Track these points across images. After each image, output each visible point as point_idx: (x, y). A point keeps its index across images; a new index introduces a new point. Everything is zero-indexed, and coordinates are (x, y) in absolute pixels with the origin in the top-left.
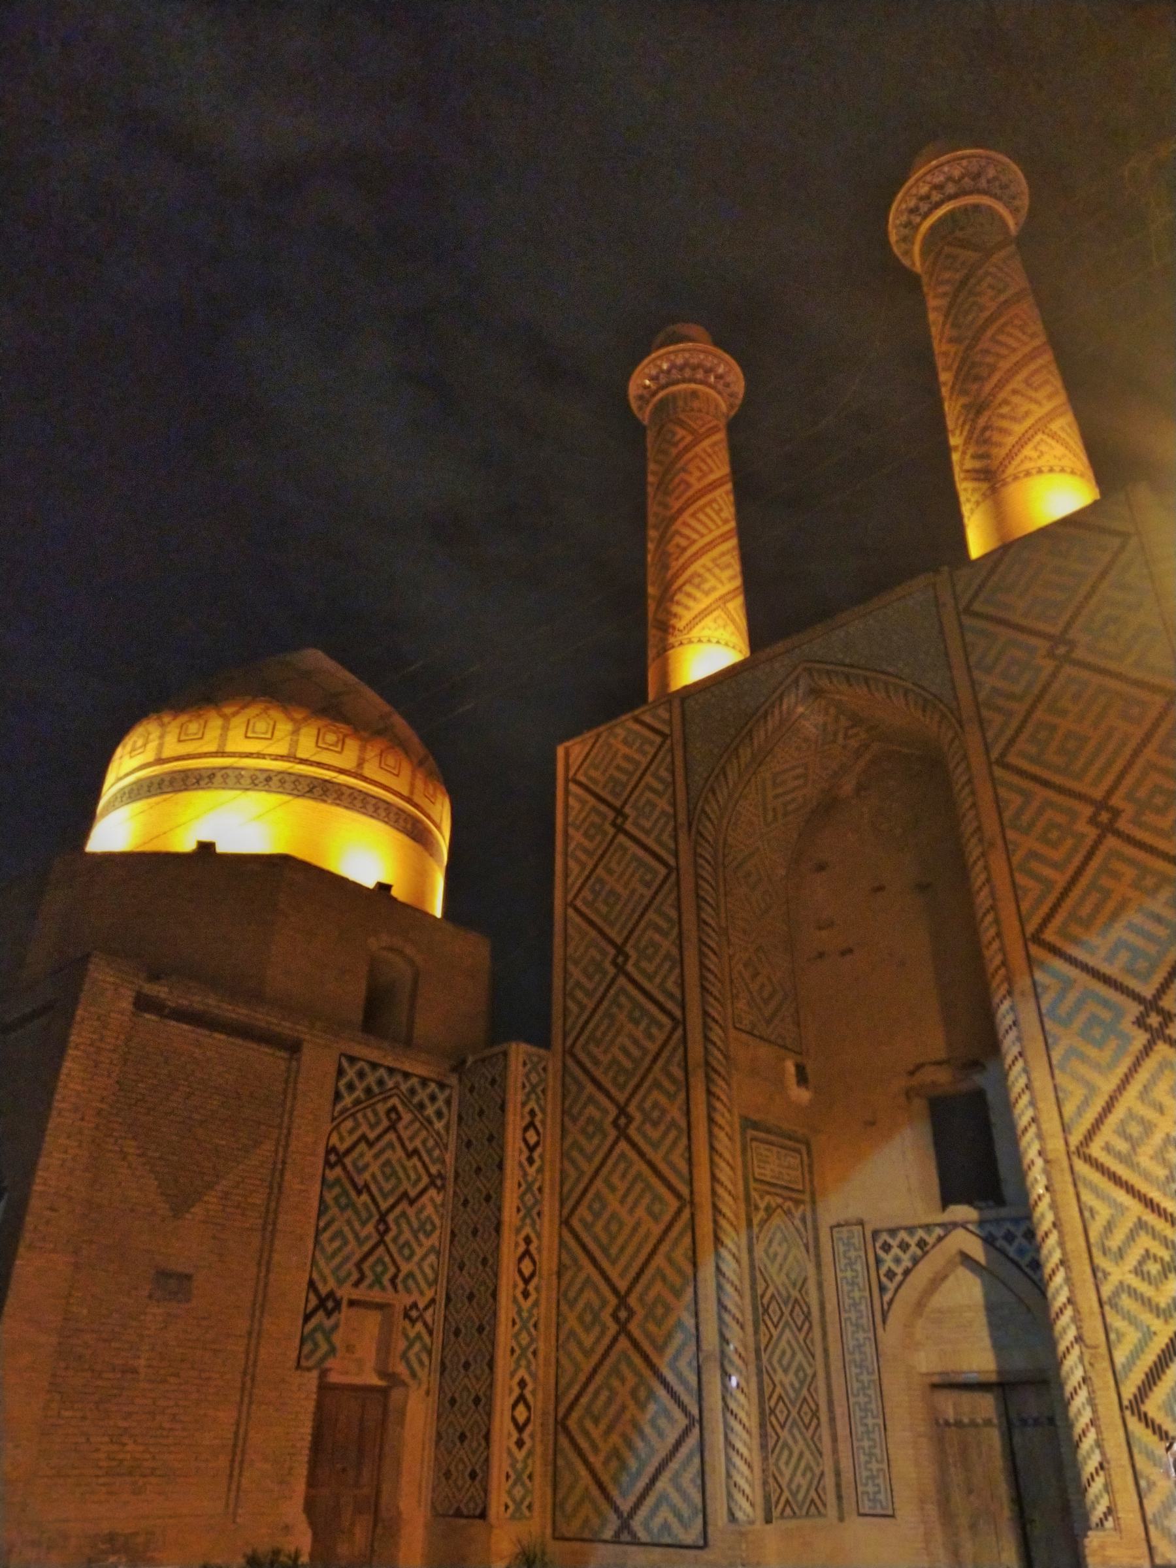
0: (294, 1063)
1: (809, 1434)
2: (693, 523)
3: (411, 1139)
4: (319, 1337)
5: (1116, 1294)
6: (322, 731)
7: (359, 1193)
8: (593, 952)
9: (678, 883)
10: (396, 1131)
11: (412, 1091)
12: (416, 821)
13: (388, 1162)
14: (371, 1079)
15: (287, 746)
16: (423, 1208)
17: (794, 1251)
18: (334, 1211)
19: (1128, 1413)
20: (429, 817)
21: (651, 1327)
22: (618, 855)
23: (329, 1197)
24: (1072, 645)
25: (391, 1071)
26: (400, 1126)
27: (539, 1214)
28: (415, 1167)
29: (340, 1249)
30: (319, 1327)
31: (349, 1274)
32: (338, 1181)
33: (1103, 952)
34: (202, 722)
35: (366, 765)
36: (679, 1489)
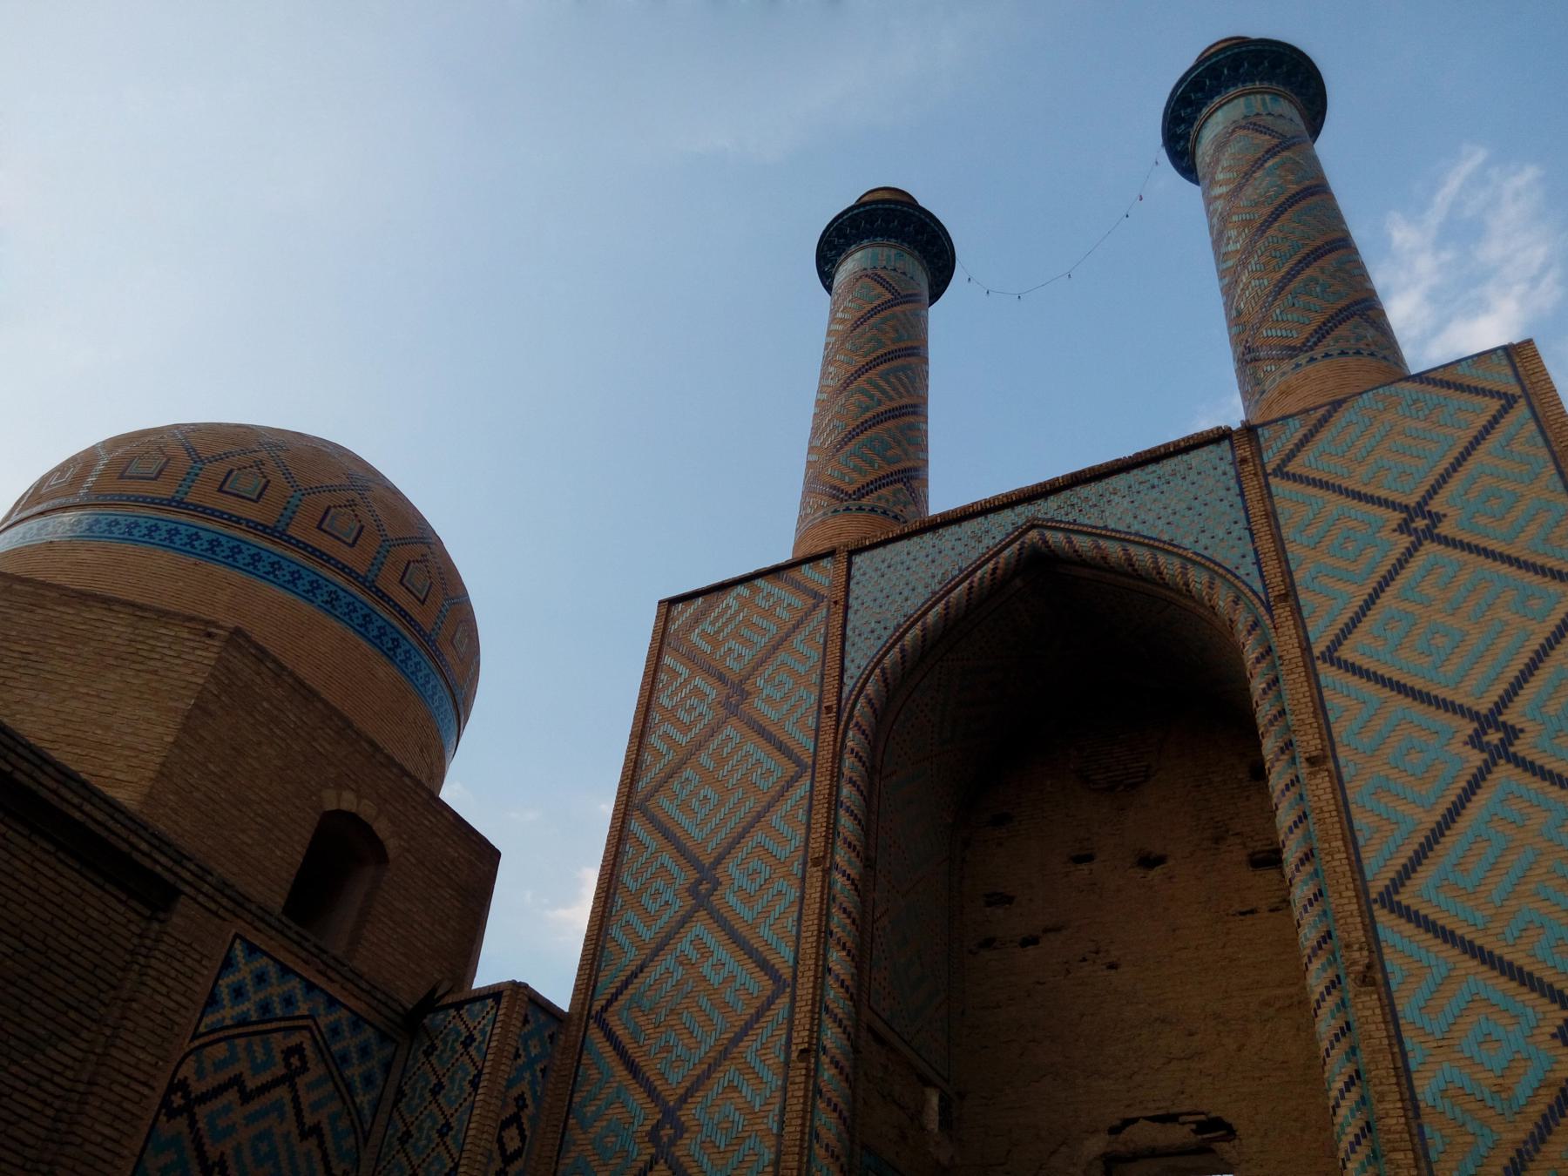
10: (293, 1088)
14: (276, 990)
25: (310, 987)
26: (301, 1081)
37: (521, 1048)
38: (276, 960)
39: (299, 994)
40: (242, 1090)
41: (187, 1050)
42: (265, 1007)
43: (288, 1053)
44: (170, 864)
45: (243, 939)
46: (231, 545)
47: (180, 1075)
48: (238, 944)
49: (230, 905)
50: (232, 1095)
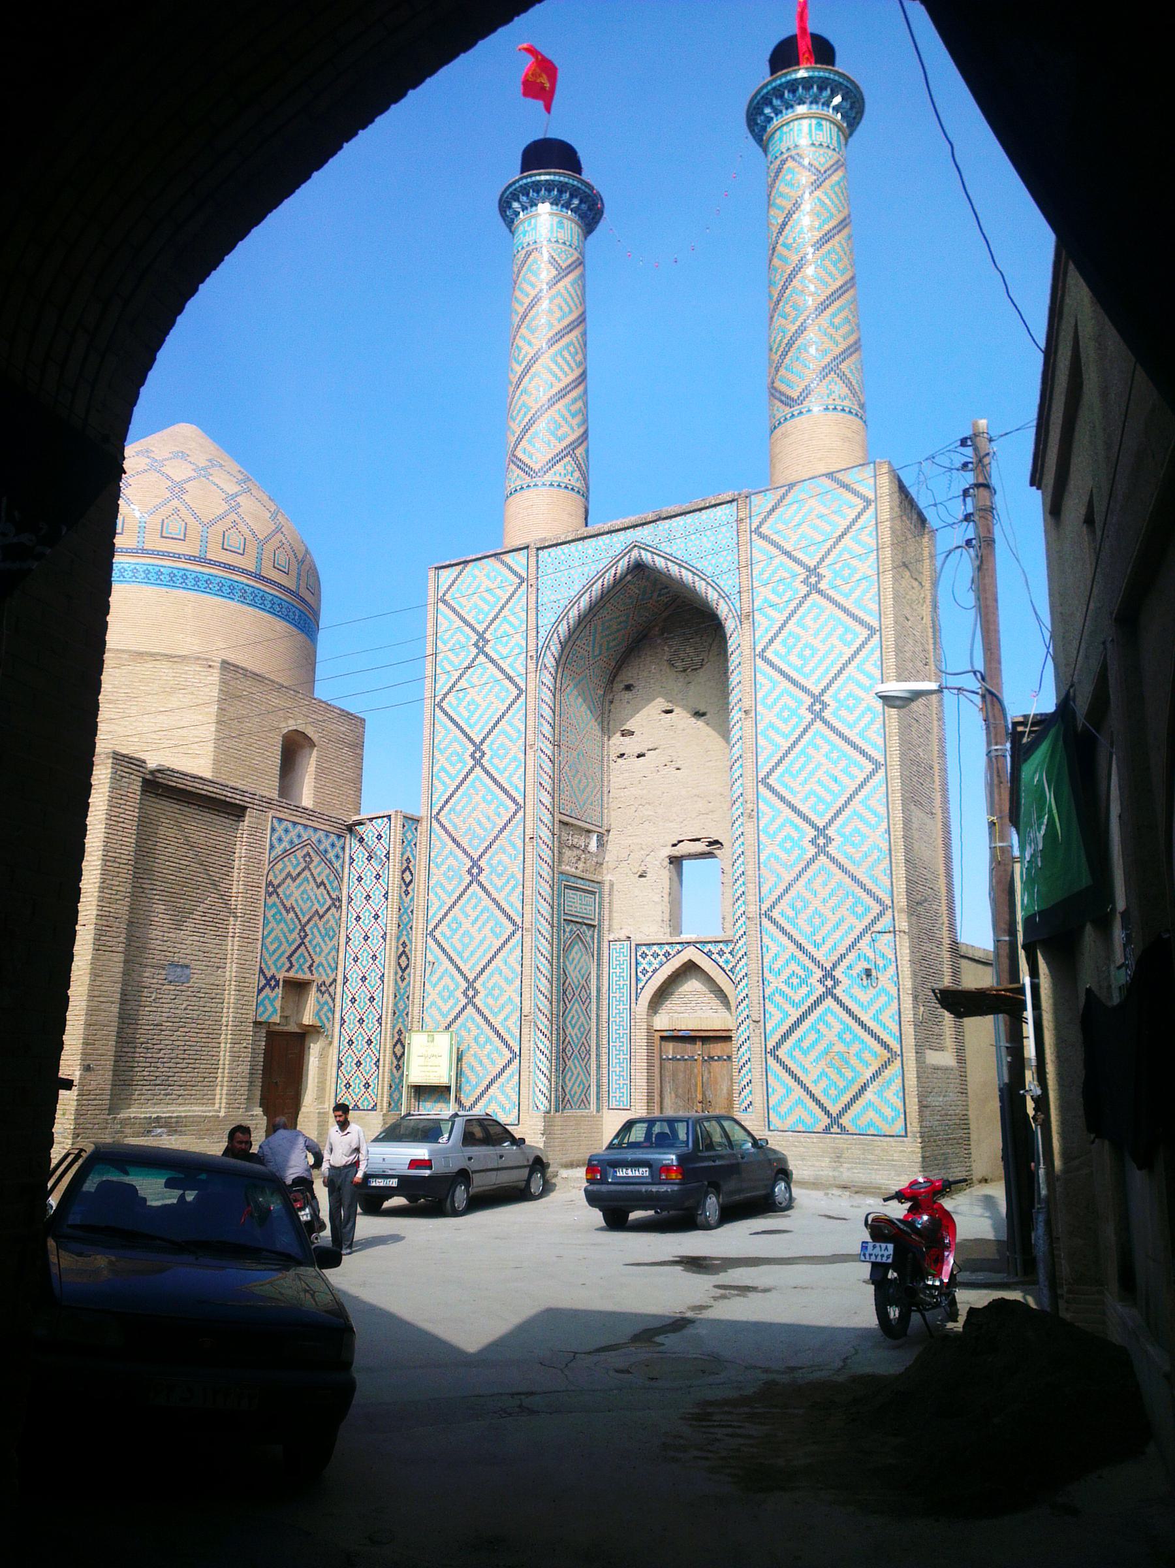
1: (583, 1064)
4: (267, 1002)
5: (773, 994)
7: (288, 912)
14: (293, 834)
16: (328, 921)
17: (584, 957)
18: (273, 924)
19: (769, 1055)
21: (490, 1001)
23: (269, 915)
24: (820, 577)
25: (306, 826)
27: (411, 928)
29: (278, 948)
30: (267, 997)
31: (284, 964)
32: (274, 904)
33: (800, 796)
36: (503, 1093)
40: (292, 878)
42: (291, 842)
43: (304, 857)
46: (180, 574)
49: (267, 805)
50: (289, 881)
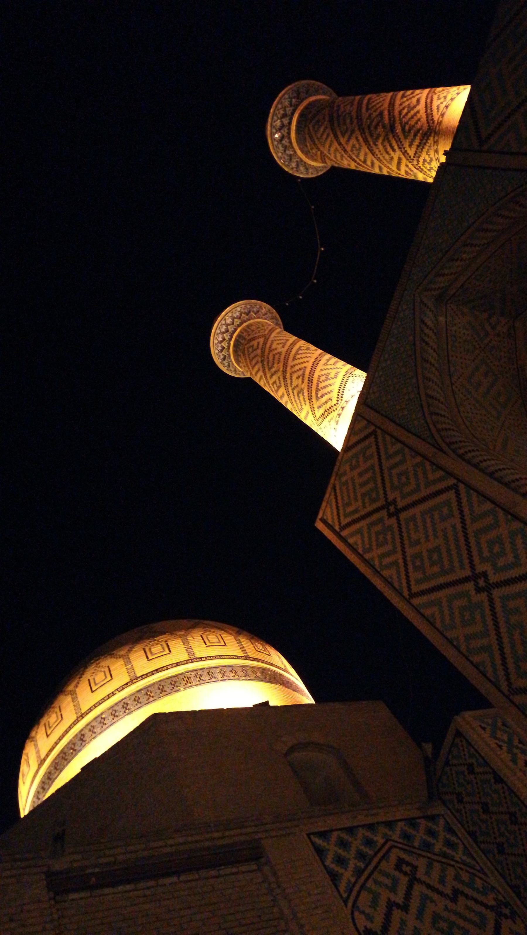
0: (266, 868)
2: (296, 362)
3: (442, 881)
6: (147, 649)
8: (458, 603)
9: (469, 486)
10: (419, 881)
11: (406, 836)
12: (264, 671)
13: (436, 918)
14: (356, 844)
15: (127, 675)
20: (272, 665)
22: (412, 526)
25: (370, 827)
26: (421, 874)
28: (467, 907)
34: (57, 710)
35: (195, 650)
37: (497, 741)
38: (341, 829)
39: (368, 834)
41: (350, 912)
42: (361, 856)
43: (398, 867)
44: (239, 831)
45: (314, 834)
47: (362, 929)
48: (312, 837)
